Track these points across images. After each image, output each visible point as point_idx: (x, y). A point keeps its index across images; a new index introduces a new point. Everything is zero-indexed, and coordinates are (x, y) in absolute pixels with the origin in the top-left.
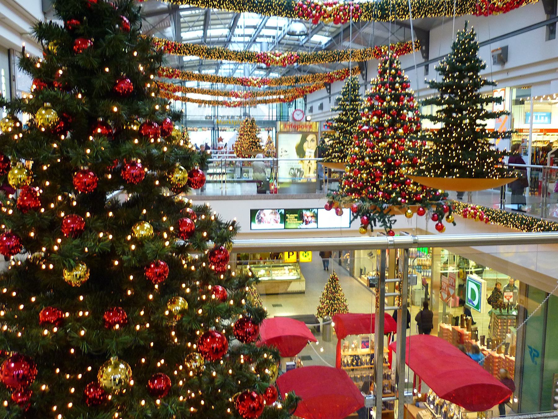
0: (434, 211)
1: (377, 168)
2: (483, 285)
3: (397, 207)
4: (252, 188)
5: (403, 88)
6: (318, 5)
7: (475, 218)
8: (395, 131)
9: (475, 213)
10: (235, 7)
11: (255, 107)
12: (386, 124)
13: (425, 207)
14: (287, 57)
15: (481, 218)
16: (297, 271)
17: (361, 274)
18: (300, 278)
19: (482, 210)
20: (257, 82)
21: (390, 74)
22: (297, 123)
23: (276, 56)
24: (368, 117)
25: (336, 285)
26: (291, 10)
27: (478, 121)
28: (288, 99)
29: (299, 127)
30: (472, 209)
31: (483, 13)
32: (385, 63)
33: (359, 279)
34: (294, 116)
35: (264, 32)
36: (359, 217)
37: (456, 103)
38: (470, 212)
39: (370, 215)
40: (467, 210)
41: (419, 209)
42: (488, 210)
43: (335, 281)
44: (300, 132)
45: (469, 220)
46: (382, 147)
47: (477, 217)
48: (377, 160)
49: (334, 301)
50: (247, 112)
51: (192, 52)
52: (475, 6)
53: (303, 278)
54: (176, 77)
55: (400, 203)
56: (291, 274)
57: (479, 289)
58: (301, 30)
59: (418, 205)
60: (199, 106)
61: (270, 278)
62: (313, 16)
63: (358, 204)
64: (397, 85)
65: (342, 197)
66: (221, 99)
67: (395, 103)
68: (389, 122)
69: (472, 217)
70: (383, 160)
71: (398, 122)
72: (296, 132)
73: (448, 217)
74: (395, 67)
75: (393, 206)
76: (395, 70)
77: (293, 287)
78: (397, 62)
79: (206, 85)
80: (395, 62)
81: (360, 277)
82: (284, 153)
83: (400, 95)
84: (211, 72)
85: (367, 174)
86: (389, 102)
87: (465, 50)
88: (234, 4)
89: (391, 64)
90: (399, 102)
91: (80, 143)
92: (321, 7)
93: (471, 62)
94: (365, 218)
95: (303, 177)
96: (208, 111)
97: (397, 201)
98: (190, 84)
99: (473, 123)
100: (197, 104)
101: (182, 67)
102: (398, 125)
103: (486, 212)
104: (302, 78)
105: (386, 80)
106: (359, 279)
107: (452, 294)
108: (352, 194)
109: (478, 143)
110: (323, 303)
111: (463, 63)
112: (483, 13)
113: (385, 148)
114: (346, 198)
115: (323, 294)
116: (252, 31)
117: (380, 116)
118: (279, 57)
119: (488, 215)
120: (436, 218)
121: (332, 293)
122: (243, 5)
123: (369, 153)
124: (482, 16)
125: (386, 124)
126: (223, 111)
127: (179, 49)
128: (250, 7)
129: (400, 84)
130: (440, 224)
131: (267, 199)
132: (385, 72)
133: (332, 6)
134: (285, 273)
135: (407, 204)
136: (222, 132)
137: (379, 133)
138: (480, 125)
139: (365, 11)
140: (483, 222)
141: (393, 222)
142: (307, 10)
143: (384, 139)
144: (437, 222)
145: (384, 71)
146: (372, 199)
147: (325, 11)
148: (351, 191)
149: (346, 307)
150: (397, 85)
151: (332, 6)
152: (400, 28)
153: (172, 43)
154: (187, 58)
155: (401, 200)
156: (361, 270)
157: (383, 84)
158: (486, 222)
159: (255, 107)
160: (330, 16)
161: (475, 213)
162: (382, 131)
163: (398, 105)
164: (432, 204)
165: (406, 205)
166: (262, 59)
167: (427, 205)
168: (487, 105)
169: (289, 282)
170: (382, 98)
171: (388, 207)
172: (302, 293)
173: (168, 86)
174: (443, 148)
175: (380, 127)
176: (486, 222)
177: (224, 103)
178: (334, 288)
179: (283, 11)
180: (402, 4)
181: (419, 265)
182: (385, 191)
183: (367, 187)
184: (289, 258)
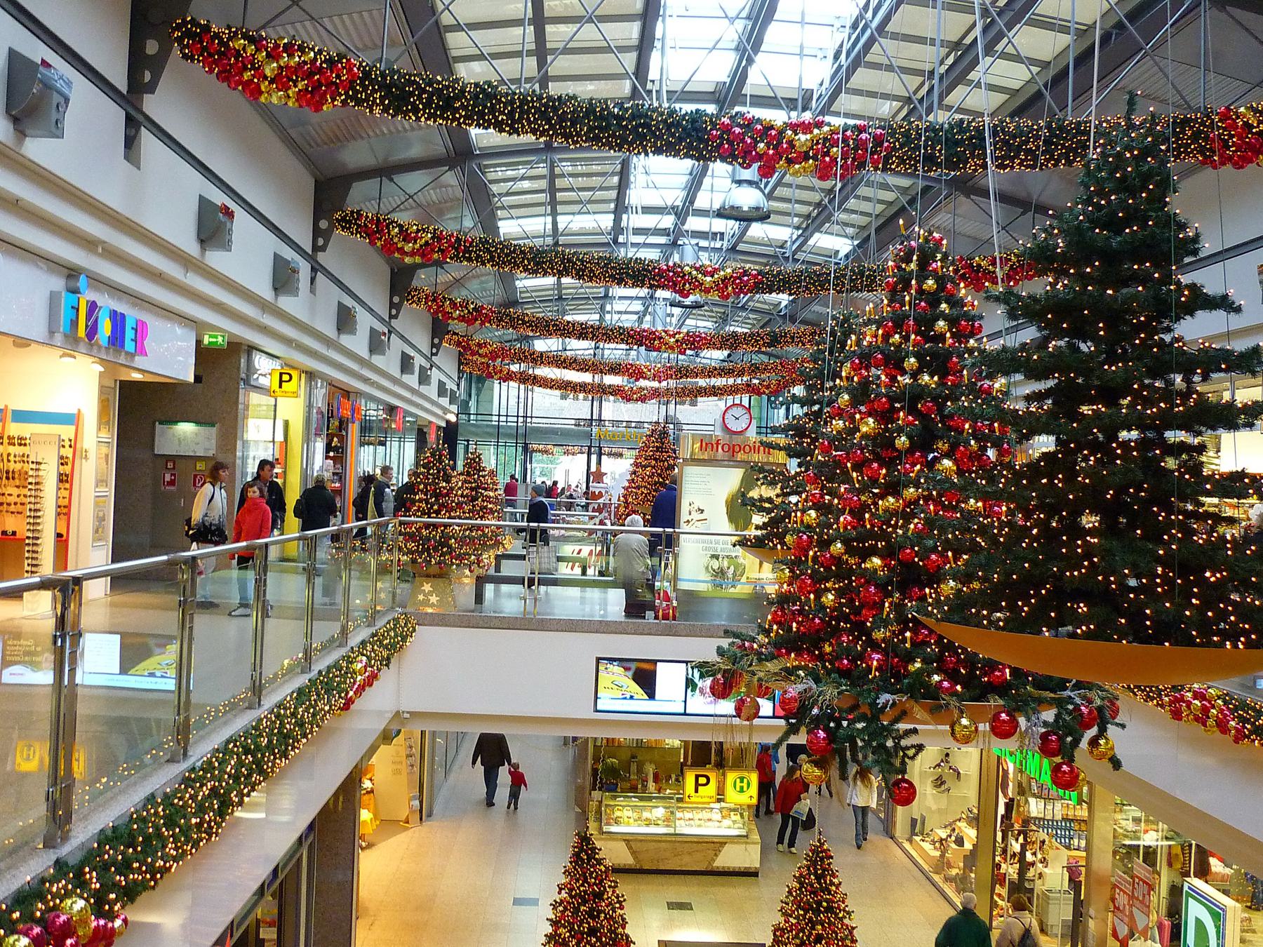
0: (1045, 724)
1: (870, 576)
2: (1229, 915)
3: (922, 706)
4: (616, 600)
5: (961, 336)
6: (772, 127)
7: (1205, 725)
8: (931, 465)
9: (1205, 710)
10: (552, 127)
11: (693, 404)
12: (902, 441)
13: (1018, 709)
14: (732, 277)
15: (1222, 726)
16: (742, 815)
17: (913, 833)
18: (747, 836)
19: (1225, 702)
20: (677, 341)
21: (920, 291)
22: (737, 440)
23: (705, 274)
24: (852, 419)
25: (824, 870)
26: (700, 140)
27: (1174, 436)
28: (768, 387)
29: (737, 449)
30: (1197, 695)
31: (1230, 159)
32: (908, 260)
33: (907, 845)
34: (726, 421)
35: (694, 223)
36: (803, 729)
37: (1085, 365)
38: (1189, 704)
39: (839, 725)
40: (1182, 699)
41: (997, 716)
42: (1244, 706)
43: (822, 859)
44: (739, 464)
45: (1189, 727)
46: (886, 510)
47: (1211, 722)
48: (873, 552)
49: (817, 912)
50: (671, 413)
51: (499, 258)
52: (1206, 139)
53: (756, 837)
54: (483, 323)
55: (932, 693)
56: (727, 822)
57: (1217, 927)
58: (753, 204)
59: (995, 702)
60: (564, 397)
61: (671, 831)
62: (759, 157)
63: (800, 687)
64: (941, 324)
65: (760, 660)
66: (610, 380)
67: (932, 377)
68: (910, 437)
69: (1197, 719)
70: (886, 555)
71: (942, 438)
72: (732, 462)
73: (1094, 742)
74: (935, 270)
75: (912, 702)
76: (937, 282)
77: (729, 858)
78: (945, 256)
79: (580, 347)
80: (939, 256)
81: (910, 840)
82: (696, 516)
83: (948, 354)
84: (589, 318)
85: (840, 593)
86: (915, 375)
87: (1124, 186)
88: (549, 121)
89: (924, 263)
90: (943, 377)
91: (1007, 498)
92: (781, 132)
93: (1144, 226)
94: (822, 734)
95: (744, 580)
96: (579, 408)
97: (927, 686)
98: (540, 345)
99: (1153, 443)
100: (558, 393)
101: (515, 303)
102: (943, 446)
103: (1236, 709)
104: (785, 337)
105: (907, 308)
106: (907, 845)
107: (1140, 926)
108: (788, 654)
109: (1170, 510)
110: (786, 915)
111: (1114, 225)
112: (1230, 159)
113: (894, 513)
114: (772, 666)
115: (790, 892)
116: (668, 221)
117: (886, 416)
118: (712, 276)
119: (1244, 720)
120: (1054, 745)
121: (814, 892)
122: (573, 124)
123: (845, 528)
124: (1229, 167)
125: (902, 441)
126: (612, 409)
127: (467, 251)
128: (591, 129)
129: (952, 321)
130: (1065, 768)
131: (642, 634)
132: (907, 286)
133: (811, 132)
134: (710, 820)
135: (960, 697)
136: (612, 460)
137: (880, 467)
138: (1183, 447)
139: (902, 147)
140: (1229, 739)
141: (911, 752)
142: (743, 141)
143: (893, 488)
144: (1058, 759)
145: (905, 282)
146: (845, 673)
147: (791, 143)
148: (787, 644)
149: (851, 933)
150: (941, 324)
151: (811, 132)
152: (1023, 214)
153: (452, 235)
154: (526, 283)
155: (941, 681)
156: (914, 822)
157: (898, 323)
158: (1236, 740)
159: (693, 404)
160: (806, 157)
161: (1205, 710)
162: (890, 463)
163: (941, 383)
164: (1040, 701)
165: (954, 702)
166: (670, 279)
167: (1026, 703)
168: (1205, 378)
169: (717, 844)
170: (894, 363)
171: (894, 703)
172: (751, 874)
173: (479, 345)
174: (1043, 526)
175: (882, 445)
176: (1236, 740)
177: (616, 391)
178: (818, 878)
179: (680, 140)
180: (1003, 130)
181: (1065, 819)
182: (889, 650)
183: (836, 632)
184: (696, 791)
